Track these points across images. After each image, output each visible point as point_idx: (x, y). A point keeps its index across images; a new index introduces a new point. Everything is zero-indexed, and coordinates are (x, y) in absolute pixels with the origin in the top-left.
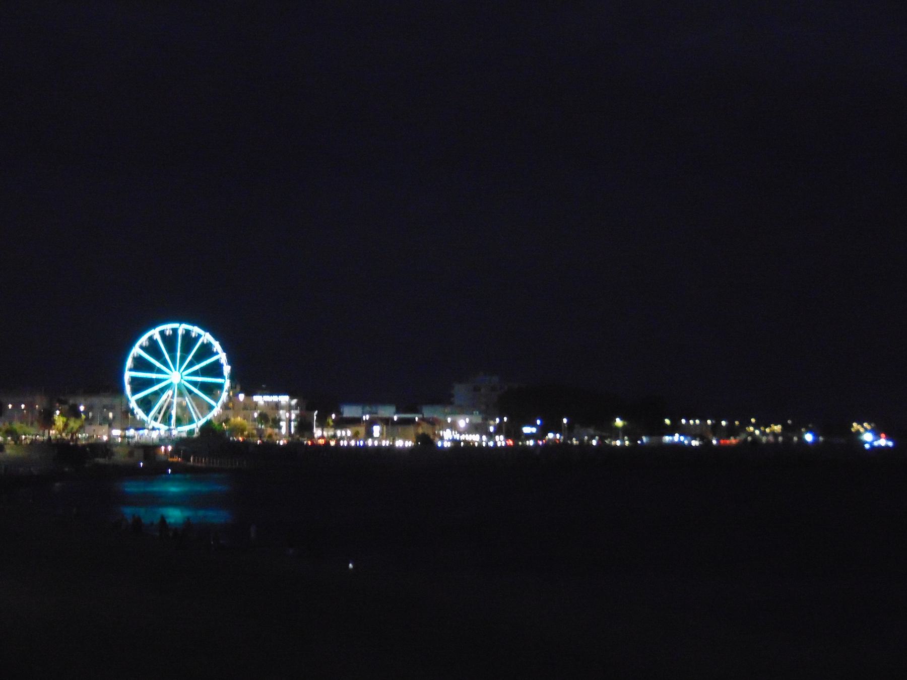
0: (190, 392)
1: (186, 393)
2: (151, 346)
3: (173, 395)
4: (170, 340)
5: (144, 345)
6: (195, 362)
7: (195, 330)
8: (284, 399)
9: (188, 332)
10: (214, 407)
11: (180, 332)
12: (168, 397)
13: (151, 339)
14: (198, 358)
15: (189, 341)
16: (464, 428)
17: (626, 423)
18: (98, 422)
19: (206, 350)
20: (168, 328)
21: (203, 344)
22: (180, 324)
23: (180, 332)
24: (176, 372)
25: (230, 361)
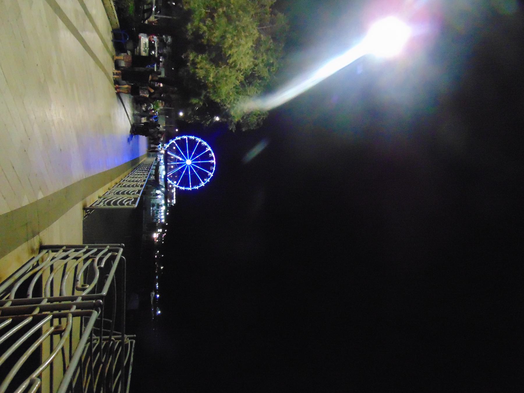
5: (202, 143)
8: (174, 201)
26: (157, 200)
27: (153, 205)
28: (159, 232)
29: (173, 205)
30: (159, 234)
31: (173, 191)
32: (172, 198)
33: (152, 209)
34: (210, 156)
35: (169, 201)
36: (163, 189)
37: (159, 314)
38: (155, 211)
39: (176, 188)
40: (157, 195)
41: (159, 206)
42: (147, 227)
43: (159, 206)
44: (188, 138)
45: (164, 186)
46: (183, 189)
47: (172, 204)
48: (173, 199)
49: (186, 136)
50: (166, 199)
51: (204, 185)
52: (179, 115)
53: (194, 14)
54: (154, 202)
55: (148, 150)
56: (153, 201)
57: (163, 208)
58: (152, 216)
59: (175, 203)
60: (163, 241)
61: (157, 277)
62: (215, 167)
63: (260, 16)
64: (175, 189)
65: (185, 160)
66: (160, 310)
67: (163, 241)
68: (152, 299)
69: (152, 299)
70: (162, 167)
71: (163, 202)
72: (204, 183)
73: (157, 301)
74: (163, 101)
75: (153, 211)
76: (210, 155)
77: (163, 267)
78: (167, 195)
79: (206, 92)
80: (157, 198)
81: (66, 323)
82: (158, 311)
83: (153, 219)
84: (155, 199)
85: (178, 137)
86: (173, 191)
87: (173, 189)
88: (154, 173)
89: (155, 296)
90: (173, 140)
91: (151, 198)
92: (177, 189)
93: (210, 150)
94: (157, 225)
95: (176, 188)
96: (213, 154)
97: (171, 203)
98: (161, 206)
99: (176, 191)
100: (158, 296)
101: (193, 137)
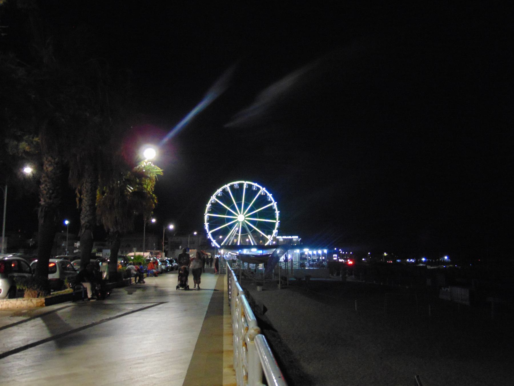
0: (254, 232)
1: (248, 230)
2: (225, 197)
3: (238, 232)
4: (237, 192)
5: (219, 195)
6: (258, 216)
8: (295, 238)
9: (250, 186)
13: (224, 191)
14: (257, 205)
15: (251, 193)
16: (321, 250)
17: (387, 254)
19: (263, 200)
21: (260, 195)
26: (294, 261)
27: (302, 265)
29: (300, 239)
33: (309, 267)
36: (278, 251)
38: (311, 263)
40: (286, 260)
41: (302, 257)
42: (335, 275)
43: (302, 257)
44: (209, 212)
45: (274, 250)
46: (279, 223)
47: (299, 240)
49: (205, 215)
50: (294, 247)
51: (276, 203)
54: (297, 264)
55: (216, 273)
56: (296, 266)
57: (307, 251)
59: (297, 237)
60: (349, 252)
61: (399, 261)
62: (253, 184)
64: (278, 237)
65: (238, 222)
66: (443, 256)
70: (245, 252)
71: (298, 251)
72: (273, 203)
73: (432, 261)
77: (385, 253)
78: (288, 246)
79: (178, 271)
80: (292, 261)
81: (105, 319)
83: (324, 266)
84: (293, 263)
85: (208, 236)
86: (282, 240)
88: (255, 265)
89: (425, 262)
90: (208, 234)
91: (292, 269)
93: (229, 185)
94: (397, 261)
96: (236, 183)
98: (302, 254)
99: (282, 236)
100: (423, 259)
101: (208, 205)
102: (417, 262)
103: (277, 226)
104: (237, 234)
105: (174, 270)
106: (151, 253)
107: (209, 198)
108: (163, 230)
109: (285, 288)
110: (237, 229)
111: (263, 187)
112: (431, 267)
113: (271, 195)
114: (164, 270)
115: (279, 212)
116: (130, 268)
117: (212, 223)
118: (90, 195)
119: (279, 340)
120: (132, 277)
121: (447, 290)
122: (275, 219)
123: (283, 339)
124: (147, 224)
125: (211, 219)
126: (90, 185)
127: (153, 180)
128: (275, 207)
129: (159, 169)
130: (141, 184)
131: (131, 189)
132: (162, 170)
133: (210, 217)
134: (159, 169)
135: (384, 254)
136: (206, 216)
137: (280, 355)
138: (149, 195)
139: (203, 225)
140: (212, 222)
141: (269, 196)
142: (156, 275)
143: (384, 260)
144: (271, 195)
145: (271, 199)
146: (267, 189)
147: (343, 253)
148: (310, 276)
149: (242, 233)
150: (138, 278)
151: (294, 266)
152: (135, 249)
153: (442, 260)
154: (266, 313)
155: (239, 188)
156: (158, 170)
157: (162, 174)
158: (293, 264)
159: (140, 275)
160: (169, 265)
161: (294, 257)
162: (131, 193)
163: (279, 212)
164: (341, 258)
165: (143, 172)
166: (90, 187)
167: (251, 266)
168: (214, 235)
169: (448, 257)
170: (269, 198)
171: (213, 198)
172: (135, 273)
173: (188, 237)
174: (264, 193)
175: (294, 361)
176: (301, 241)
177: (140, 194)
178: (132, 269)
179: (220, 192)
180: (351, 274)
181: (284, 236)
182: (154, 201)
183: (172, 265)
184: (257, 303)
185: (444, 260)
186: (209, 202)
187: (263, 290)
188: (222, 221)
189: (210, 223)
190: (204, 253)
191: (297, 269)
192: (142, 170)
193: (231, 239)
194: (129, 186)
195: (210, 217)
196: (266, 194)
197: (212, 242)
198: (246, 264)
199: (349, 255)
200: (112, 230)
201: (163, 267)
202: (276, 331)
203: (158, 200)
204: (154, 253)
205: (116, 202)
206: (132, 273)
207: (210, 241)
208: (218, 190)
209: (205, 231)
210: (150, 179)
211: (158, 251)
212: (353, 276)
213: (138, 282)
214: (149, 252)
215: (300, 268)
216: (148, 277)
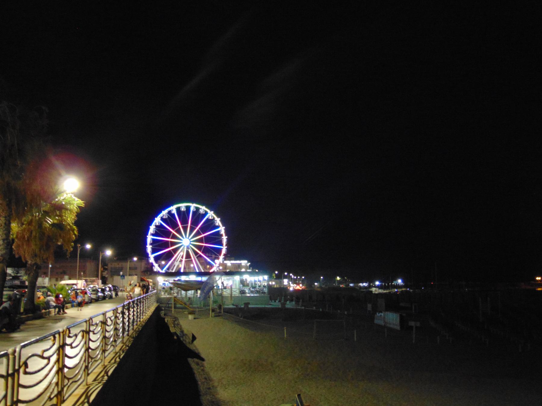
3: (182, 257)
5: (164, 217)
7: (203, 209)
8: (244, 262)
10: (214, 266)
11: (192, 209)
12: (182, 257)
13: (170, 212)
17: (340, 278)
18: (128, 273)
20: (183, 206)
22: (50, 301)
23: (192, 209)
24: (184, 239)
25: (227, 233)
27: (242, 292)
28: (288, 282)
29: (249, 264)
30: (291, 283)
31: (230, 265)
32: (239, 266)
33: (249, 294)
34: (185, 210)
35: (243, 270)
37: (403, 281)
39: (225, 259)
42: (277, 301)
44: (153, 235)
46: (226, 248)
48: (241, 264)
51: (224, 228)
52: (87, 248)
53: (208, 285)
58: (259, 294)
59: (246, 262)
63: (69, 217)
64: (225, 262)
66: (396, 279)
67: (301, 277)
68: (381, 291)
69: (381, 291)
73: (385, 285)
74: (3, 289)
75: (252, 292)
76: (184, 209)
82: (398, 282)
84: (233, 289)
87: (226, 264)
89: (378, 287)
92: (227, 257)
94: (350, 285)
95: (225, 259)
97: (246, 267)
99: (230, 260)
100: (377, 283)
102: (370, 287)
103: (223, 232)
104: (182, 259)
105: (107, 299)
106: (86, 281)
107: (153, 220)
108: (99, 256)
109: (219, 316)
110: (182, 254)
111: (211, 210)
112: (384, 290)
113: (219, 219)
114: (94, 299)
115: (227, 237)
116: (49, 299)
117: (155, 246)
118: (4, 229)
119: (202, 368)
120: (51, 308)
121: (381, 315)
122: (222, 245)
123: (206, 368)
124: (81, 250)
125: (154, 242)
126: (4, 219)
127: (73, 213)
128: (223, 232)
129: (80, 200)
130: (60, 216)
131: (50, 221)
132: (83, 202)
133: (153, 240)
134: (79, 201)
135: (337, 278)
136: (150, 238)
137: (200, 383)
138: (69, 227)
139: (145, 248)
140: (154, 245)
141: (216, 220)
142: (80, 305)
143: (337, 285)
144: (219, 219)
145: (218, 224)
146: (215, 213)
147: (295, 277)
148: (248, 304)
149: (186, 258)
150: (57, 310)
151: (234, 293)
152: (66, 277)
153: (395, 283)
154: (195, 342)
155: (186, 210)
156: (79, 202)
157: (83, 205)
158: (233, 291)
159: (61, 306)
160: (100, 294)
161: (234, 283)
162: (50, 225)
163: (227, 237)
164: (293, 283)
165: (63, 204)
166: (4, 222)
167: (189, 294)
168: (157, 259)
169: (402, 280)
170: (216, 222)
171: (158, 220)
172: (54, 304)
173: (127, 262)
174: (212, 217)
175: (212, 388)
176: (250, 265)
177: (59, 226)
178: (51, 300)
179: (166, 214)
180: (292, 300)
181: (232, 260)
182: (74, 232)
183: (104, 294)
184: (185, 332)
185: (396, 284)
186: (154, 224)
187: (195, 318)
188: (166, 245)
189: (152, 246)
190: (145, 279)
191: (237, 296)
192: (62, 202)
193: (176, 264)
194: (48, 218)
195: (153, 240)
196: (214, 218)
197: (154, 266)
198: (183, 292)
199: (301, 279)
200: (30, 262)
201: (94, 296)
202: (203, 360)
203: (79, 231)
204: (89, 280)
205: (34, 234)
206: (50, 305)
207: (152, 265)
208: (163, 212)
209: (148, 254)
210: (71, 211)
211: (94, 278)
212: (294, 303)
213: (57, 314)
214: (83, 279)
215: (240, 295)
216: (72, 308)
